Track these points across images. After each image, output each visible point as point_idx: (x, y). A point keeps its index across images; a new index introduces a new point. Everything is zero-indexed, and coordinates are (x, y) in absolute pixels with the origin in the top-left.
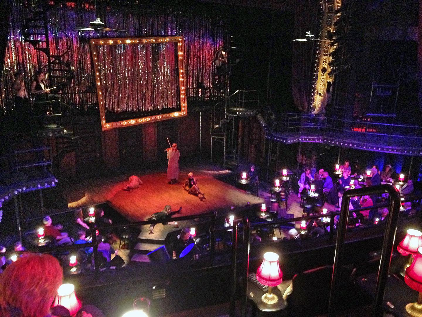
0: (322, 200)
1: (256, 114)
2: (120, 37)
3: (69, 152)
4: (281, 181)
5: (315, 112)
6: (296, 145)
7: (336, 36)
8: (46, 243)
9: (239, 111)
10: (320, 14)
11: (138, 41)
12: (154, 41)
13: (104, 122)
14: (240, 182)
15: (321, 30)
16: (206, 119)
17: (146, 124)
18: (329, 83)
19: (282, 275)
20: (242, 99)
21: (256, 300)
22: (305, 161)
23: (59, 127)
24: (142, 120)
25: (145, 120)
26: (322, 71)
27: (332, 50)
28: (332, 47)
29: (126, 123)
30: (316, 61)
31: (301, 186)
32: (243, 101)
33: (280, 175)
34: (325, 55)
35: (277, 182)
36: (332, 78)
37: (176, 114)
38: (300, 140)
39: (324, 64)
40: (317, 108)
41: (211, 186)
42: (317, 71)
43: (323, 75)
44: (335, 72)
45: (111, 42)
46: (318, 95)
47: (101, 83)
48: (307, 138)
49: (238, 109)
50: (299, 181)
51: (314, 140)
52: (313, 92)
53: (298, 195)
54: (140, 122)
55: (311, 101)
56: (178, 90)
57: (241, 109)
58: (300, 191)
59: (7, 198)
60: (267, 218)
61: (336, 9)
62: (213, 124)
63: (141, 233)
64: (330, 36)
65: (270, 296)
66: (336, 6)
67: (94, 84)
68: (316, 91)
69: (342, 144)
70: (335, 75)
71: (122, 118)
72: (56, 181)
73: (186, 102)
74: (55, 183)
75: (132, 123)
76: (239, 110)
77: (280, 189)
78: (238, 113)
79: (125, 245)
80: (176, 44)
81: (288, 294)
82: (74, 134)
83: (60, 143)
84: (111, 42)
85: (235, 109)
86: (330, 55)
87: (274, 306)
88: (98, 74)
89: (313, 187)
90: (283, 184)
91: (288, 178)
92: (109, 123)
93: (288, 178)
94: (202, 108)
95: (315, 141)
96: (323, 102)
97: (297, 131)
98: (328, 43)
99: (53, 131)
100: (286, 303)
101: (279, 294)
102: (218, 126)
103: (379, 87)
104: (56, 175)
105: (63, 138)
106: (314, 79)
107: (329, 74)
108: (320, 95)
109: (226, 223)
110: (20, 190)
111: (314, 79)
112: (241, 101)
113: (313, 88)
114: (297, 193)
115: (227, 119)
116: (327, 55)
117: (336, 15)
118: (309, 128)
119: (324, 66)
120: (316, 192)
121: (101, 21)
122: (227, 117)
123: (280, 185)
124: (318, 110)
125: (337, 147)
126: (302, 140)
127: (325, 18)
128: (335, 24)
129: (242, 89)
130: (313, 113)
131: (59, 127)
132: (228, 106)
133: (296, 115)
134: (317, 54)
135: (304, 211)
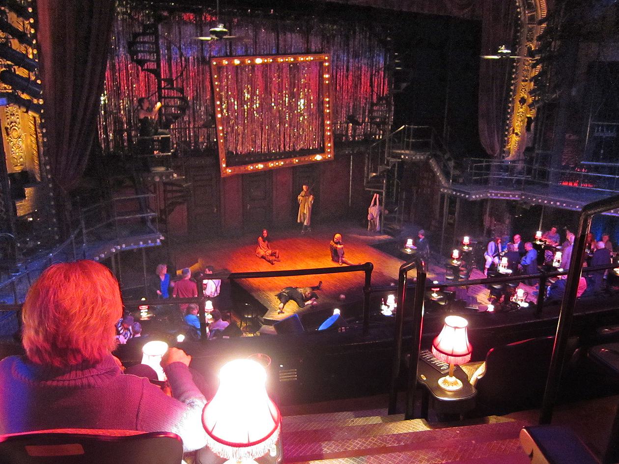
0: (519, 277)
1: (428, 159)
2: (247, 55)
3: (180, 203)
4: (461, 253)
5: (509, 158)
6: (483, 202)
7: (540, 55)
8: (148, 317)
9: (405, 155)
10: (517, 24)
11: (271, 61)
12: (292, 60)
13: (224, 165)
14: (403, 251)
15: (519, 47)
16: (359, 170)
17: (278, 169)
18: (529, 118)
19: (470, 350)
20: (408, 137)
21: (430, 385)
22: (495, 225)
23: (168, 170)
24: (272, 165)
25: (277, 164)
26: (520, 101)
27: (535, 72)
28: (534, 69)
29: (252, 168)
30: (512, 88)
31: (489, 259)
32: (411, 140)
33: (460, 244)
34: (523, 81)
35: (456, 253)
36: (534, 111)
37: (318, 157)
38: (489, 195)
39: (523, 93)
40: (512, 153)
41: (363, 255)
42: (513, 101)
43: (522, 108)
44: (539, 103)
45: (237, 62)
46: (515, 135)
47: (222, 115)
48: (498, 193)
49: (403, 152)
50: (486, 253)
51: (508, 195)
52: (507, 130)
53: (484, 273)
54: (270, 166)
55: (504, 143)
56: (323, 125)
57: (407, 152)
58: (487, 266)
59: (103, 256)
60: (440, 300)
61: (540, 18)
62: (368, 171)
63: (268, 312)
64: (531, 54)
65: (453, 379)
66: (540, 15)
67: (214, 116)
68: (512, 128)
69: (546, 202)
70: (539, 109)
71: (246, 161)
72: (162, 238)
73: (332, 140)
74: (161, 240)
75: (260, 168)
76: (406, 154)
77: (459, 263)
78: (402, 157)
79: (247, 327)
80: (321, 64)
81: (479, 377)
82: (186, 181)
83: (169, 191)
84: (237, 62)
85: (399, 152)
86: (531, 81)
87: (456, 393)
88: (218, 103)
89: (505, 261)
90: (463, 256)
91: (471, 249)
92: (231, 167)
93: (471, 249)
94: (353, 150)
95: (510, 197)
96: (520, 144)
97: (484, 183)
98: (529, 65)
99: (161, 175)
100: (474, 391)
101: (464, 378)
102: (374, 174)
103: (598, 126)
104: (164, 232)
105: (172, 184)
106: (509, 113)
107: (530, 106)
108: (517, 134)
109: (382, 304)
110: (119, 247)
111: (509, 113)
112: (408, 140)
113: (507, 125)
114: (483, 269)
115: (388, 165)
116: (526, 81)
117: (539, 26)
118: (501, 178)
119: (522, 95)
120: (508, 267)
121: (225, 27)
122: (388, 162)
123: (460, 256)
124: (514, 156)
125: (538, 208)
126: (491, 195)
127: (525, 30)
128: (540, 38)
129: (409, 124)
130: (506, 159)
131: (168, 170)
132: (389, 148)
133: (483, 161)
134: (513, 79)
135: (491, 293)
